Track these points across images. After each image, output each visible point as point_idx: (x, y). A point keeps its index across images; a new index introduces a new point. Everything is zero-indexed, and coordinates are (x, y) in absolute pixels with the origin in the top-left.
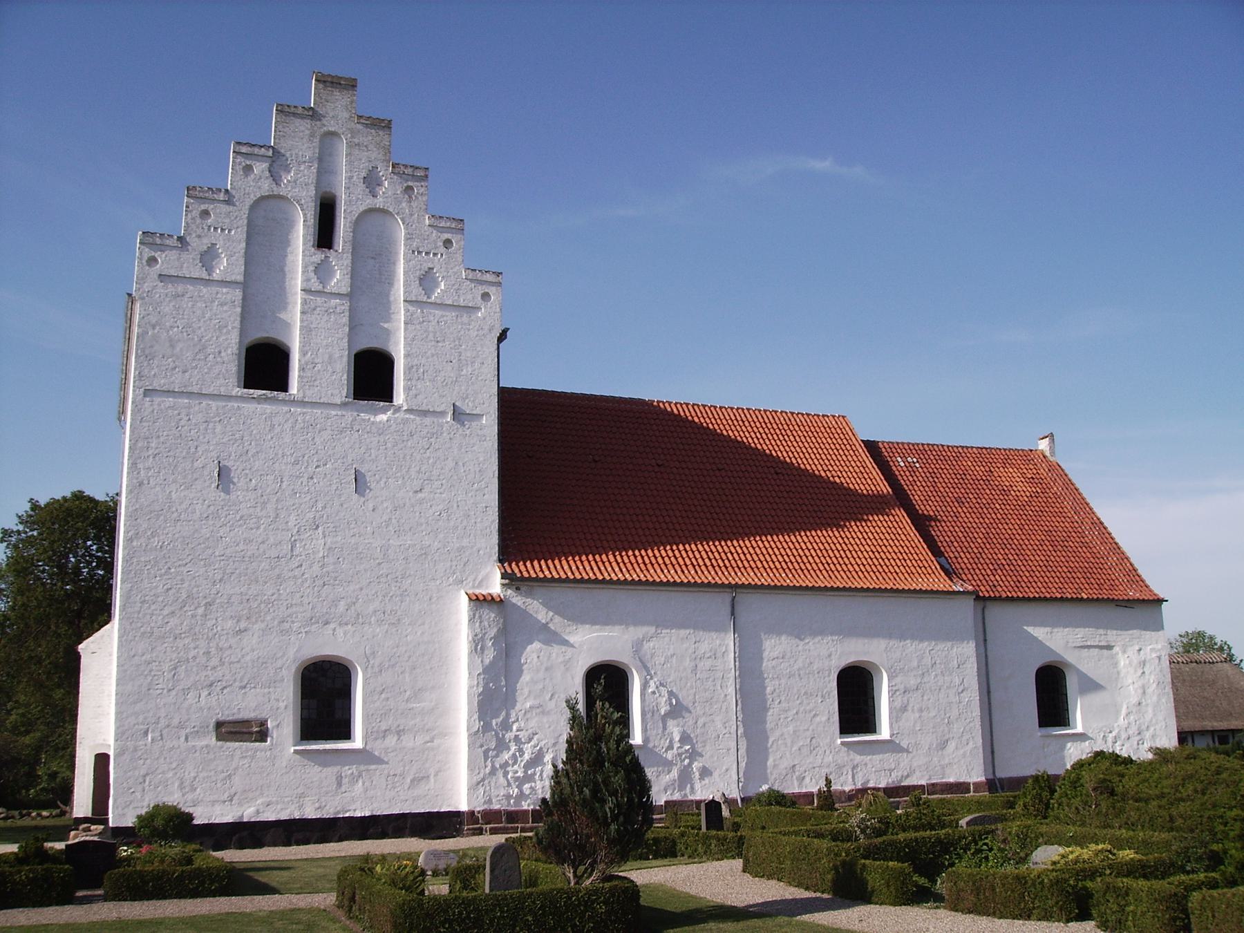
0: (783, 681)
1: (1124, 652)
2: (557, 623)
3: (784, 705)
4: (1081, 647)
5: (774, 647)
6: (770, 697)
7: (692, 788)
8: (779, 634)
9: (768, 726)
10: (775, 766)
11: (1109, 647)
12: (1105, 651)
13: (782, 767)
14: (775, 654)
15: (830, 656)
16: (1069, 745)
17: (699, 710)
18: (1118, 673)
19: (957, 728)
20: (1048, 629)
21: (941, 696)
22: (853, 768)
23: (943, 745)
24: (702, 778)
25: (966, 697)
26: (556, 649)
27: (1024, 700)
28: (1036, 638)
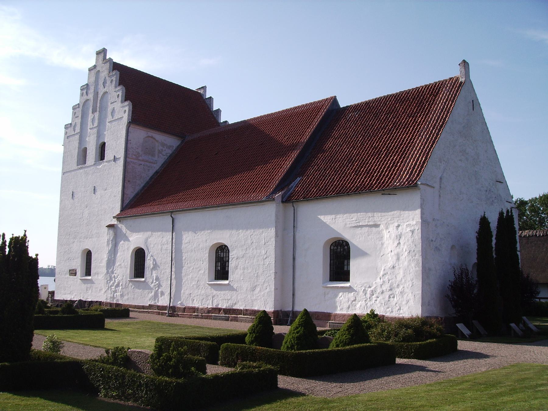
0: (189, 254)
1: (387, 228)
2: (128, 233)
3: (189, 265)
4: (355, 227)
5: (187, 237)
6: (184, 261)
7: (158, 300)
8: (188, 231)
9: (183, 274)
10: (184, 293)
11: (377, 226)
12: (374, 229)
13: (186, 294)
14: (186, 241)
15: (206, 241)
16: (341, 294)
17: (162, 267)
18: (382, 244)
19: (261, 280)
20: (333, 216)
21: (255, 261)
22: (213, 297)
23: (253, 289)
24: (161, 296)
25: (267, 262)
26: (127, 242)
27: (315, 262)
28: (325, 223)
